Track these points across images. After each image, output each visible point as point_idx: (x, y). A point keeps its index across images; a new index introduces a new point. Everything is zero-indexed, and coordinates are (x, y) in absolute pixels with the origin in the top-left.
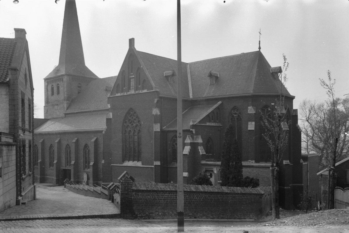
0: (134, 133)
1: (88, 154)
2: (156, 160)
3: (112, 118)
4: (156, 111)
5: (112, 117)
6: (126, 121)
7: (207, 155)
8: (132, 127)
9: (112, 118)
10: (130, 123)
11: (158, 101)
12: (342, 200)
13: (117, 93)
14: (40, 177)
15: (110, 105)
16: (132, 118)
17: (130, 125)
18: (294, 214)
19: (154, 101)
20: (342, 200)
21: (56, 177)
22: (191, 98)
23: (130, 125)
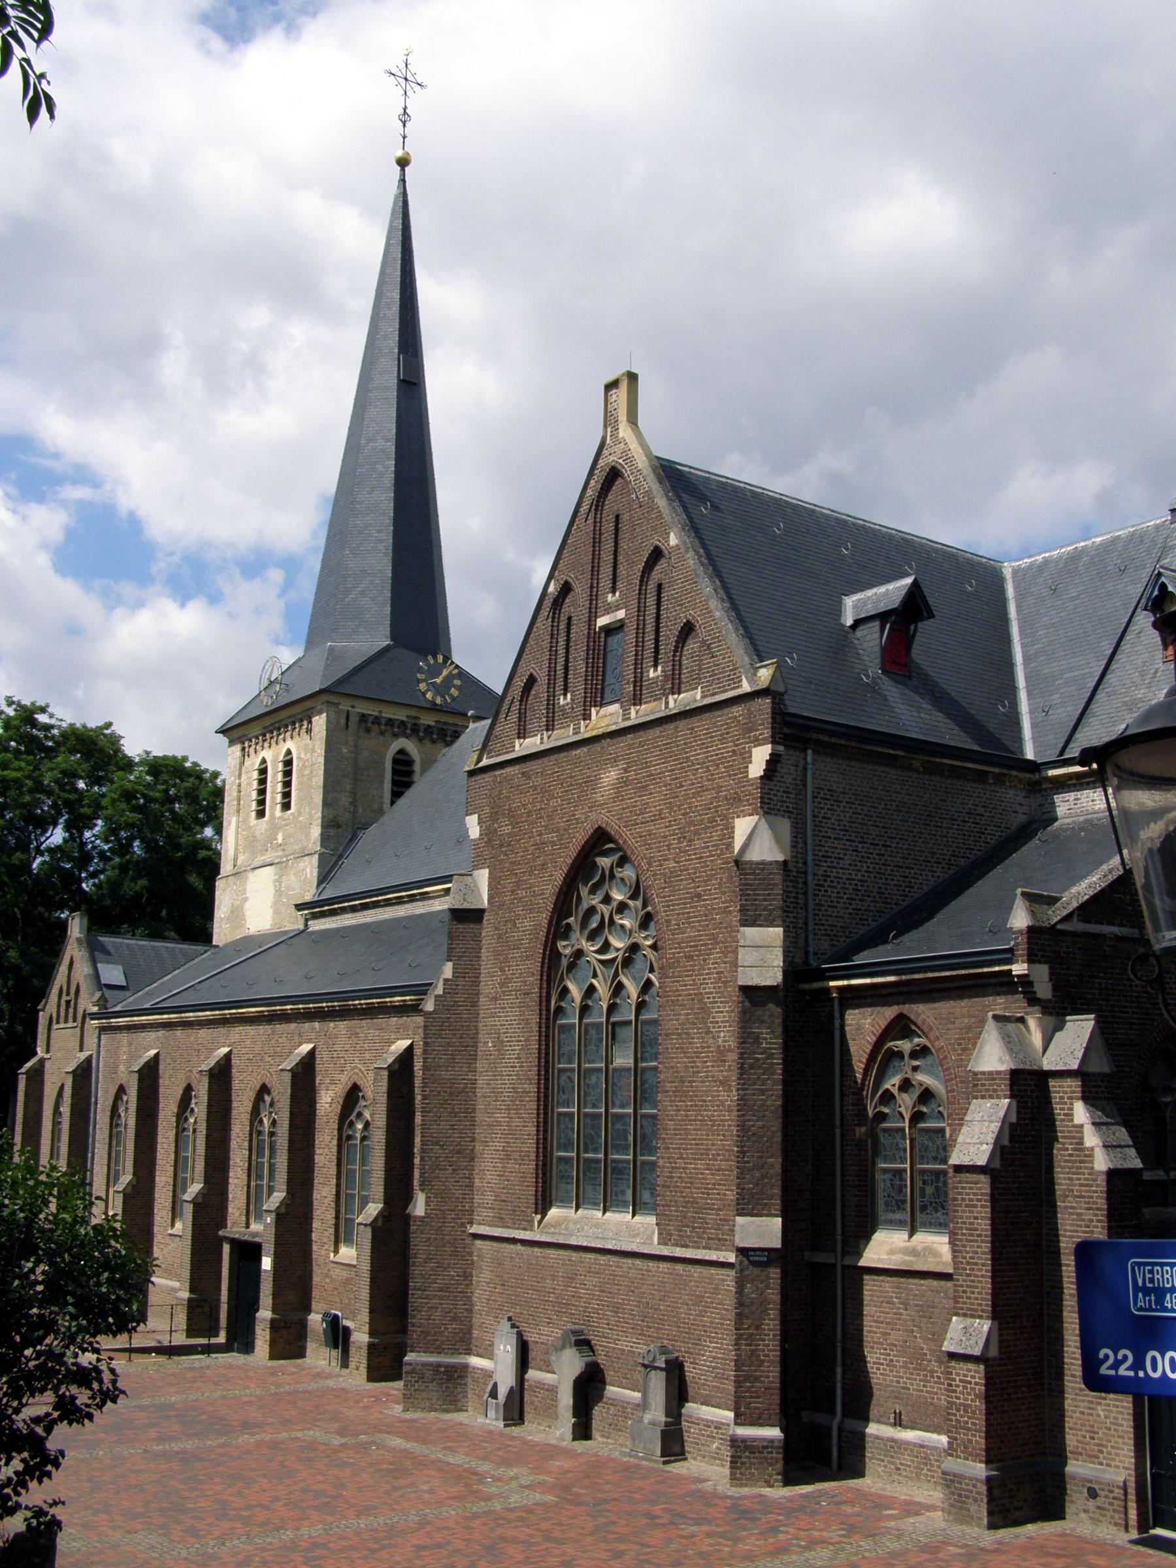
0: (612, 1008)
1: (363, 1147)
2: (748, 1205)
3: (485, 903)
4: (753, 836)
5: (490, 898)
6: (568, 925)
7: (1147, 1176)
8: (602, 962)
9: (485, 903)
10: (592, 937)
11: (773, 762)
12: (107, 1206)
13: (522, 734)
14: (872, 1429)
15: (480, 822)
16: (607, 900)
17: (590, 948)
18: (1150, 789)
19: (747, 759)
20: (107, 1206)
21: (372, 1333)
22: (1141, 833)
23: (590, 948)
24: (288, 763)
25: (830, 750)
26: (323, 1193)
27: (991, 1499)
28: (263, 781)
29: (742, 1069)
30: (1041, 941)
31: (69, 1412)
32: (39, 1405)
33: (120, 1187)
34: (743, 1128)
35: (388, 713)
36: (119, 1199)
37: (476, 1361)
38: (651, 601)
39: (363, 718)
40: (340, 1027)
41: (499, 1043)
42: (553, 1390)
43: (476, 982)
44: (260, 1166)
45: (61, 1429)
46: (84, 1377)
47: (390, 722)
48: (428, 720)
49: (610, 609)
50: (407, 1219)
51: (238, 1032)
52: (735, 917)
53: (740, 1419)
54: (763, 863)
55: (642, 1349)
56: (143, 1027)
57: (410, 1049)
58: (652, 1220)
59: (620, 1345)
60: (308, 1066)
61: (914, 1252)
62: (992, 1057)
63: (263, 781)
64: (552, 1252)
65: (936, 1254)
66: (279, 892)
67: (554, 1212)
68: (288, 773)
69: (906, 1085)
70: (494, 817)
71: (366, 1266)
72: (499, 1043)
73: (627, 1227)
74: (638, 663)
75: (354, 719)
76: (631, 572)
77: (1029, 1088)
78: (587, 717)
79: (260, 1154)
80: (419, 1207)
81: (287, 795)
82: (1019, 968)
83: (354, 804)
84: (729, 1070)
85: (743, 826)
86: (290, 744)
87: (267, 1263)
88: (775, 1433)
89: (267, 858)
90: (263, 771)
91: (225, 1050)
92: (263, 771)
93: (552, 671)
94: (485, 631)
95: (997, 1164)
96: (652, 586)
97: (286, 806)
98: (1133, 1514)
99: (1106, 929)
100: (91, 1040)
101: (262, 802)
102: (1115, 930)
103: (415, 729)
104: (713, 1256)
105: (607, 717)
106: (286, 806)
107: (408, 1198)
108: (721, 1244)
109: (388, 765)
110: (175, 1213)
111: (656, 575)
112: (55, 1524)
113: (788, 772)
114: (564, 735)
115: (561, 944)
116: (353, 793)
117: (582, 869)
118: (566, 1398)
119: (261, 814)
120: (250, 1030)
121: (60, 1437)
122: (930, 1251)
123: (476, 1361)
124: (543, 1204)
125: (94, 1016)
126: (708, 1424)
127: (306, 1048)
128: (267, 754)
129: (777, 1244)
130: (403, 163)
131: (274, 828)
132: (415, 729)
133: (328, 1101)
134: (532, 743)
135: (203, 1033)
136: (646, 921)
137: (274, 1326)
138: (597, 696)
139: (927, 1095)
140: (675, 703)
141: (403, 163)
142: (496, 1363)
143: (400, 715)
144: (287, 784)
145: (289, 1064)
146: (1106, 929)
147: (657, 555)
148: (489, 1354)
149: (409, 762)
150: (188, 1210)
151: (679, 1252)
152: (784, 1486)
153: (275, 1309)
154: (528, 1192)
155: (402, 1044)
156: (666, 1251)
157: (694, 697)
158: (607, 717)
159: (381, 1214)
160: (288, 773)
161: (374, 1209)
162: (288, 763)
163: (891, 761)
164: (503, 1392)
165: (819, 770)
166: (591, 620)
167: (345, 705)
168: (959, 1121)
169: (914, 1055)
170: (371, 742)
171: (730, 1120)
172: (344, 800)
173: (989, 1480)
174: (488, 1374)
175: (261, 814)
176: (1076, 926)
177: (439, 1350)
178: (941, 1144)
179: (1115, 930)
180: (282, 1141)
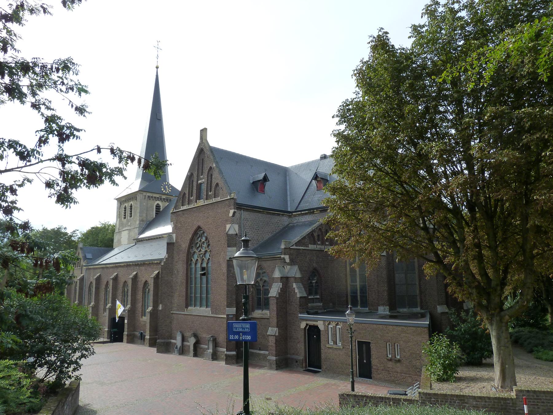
11: (234, 213)
21: (150, 336)
24: (131, 206)
25: (247, 210)
26: (139, 305)
27: (276, 364)
28: (125, 211)
29: (228, 277)
30: (287, 250)
31: (83, 356)
32: (78, 354)
33: (91, 305)
34: (227, 289)
35: (155, 195)
36: (91, 309)
37: (173, 341)
38: (209, 178)
39: (149, 197)
40: (143, 268)
41: (178, 272)
42: (189, 346)
43: (173, 258)
44: (124, 300)
45: (83, 359)
46: (86, 349)
47: (155, 197)
48: (164, 197)
49: (201, 179)
50: (158, 310)
51: (119, 269)
52: (226, 245)
53: (227, 351)
54: (232, 234)
55: (208, 337)
56: (96, 268)
57: (159, 273)
58: (210, 309)
59: (205, 336)
60: (136, 276)
61: (263, 314)
62: (277, 274)
63: (125, 211)
64: (189, 317)
65: (267, 315)
66: (129, 236)
67: (189, 308)
68: (131, 209)
69: (261, 279)
70: (177, 223)
71: (148, 321)
72: (178, 272)
73: (204, 311)
74: (207, 191)
75: (147, 197)
76: (206, 171)
77: (285, 280)
78: (196, 202)
79: (125, 296)
80: (160, 308)
81: (131, 214)
82: (282, 256)
83: (147, 216)
84: (225, 277)
85: (228, 226)
86: (132, 202)
87: (126, 321)
88: (234, 353)
89: (126, 228)
90: (125, 208)
91: (116, 274)
92: (125, 208)
93: (189, 192)
94: (177, 176)
95: (278, 296)
96: (210, 175)
97: (131, 216)
98: (304, 365)
99: (301, 248)
100: (84, 271)
101: (125, 213)
102: (303, 248)
103: (161, 199)
104: (222, 316)
105: (201, 203)
106: (131, 216)
107: (158, 306)
108: (224, 314)
109: (155, 207)
110: (105, 310)
111: (211, 172)
112: (80, 379)
113: (237, 215)
114: (192, 206)
115: (191, 250)
116: (147, 214)
117: (195, 233)
118: (192, 348)
119: (125, 218)
120: (122, 269)
121: (83, 361)
122: (266, 314)
123: (173, 341)
124: (187, 307)
125: (84, 266)
126: (221, 352)
127: (135, 273)
128: (126, 204)
129: (235, 313)
130: (157, 68)
131: (128, 221)
132: (161, 199)
133: (140, 285)
134: (185, 207)
135: (111, 270)
136: (208, 245)
137: (127, 335)
138: (199, 197)
139: (265, 281)
140: (214, 200)
141: (157, 68)
142: (178, 341)
143: (157, 196)
144: (131, 211)
145: (131, 276)
146: (301, 248)
147: (211, 168)
148: (175, 339)
149: (160, 206)
150: (107, 311)
151: (215, 316)
152: (277, 369)
153: (128, 332)
154: (184, 304)
155: (156, 272)
156: (212, 315)
157: (219, 199)
158: (201, 203)
159: (152, 309)
160: (131, 209)
161: (150, 308)
162: (131, 206)
163: (259, 212)
164: (179, 347)
165: (245, 215)
166: (197, 182)
167: (144, 194)
168: (271, 287)
169: (263, 273)
170: (151, 202)
171: (225, 287)
172: (144, 215)
173: (276, 360)
174: (175, 344)
175: (125, 218)
176: (294, 247)
177: (165, 339)
178: (267, 292)
179: (303, 248)
180: (130, 294)
